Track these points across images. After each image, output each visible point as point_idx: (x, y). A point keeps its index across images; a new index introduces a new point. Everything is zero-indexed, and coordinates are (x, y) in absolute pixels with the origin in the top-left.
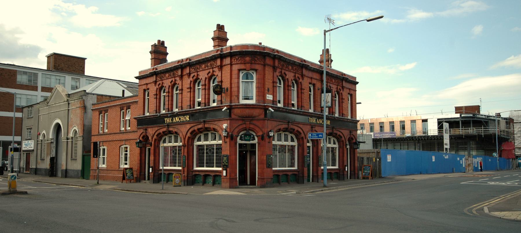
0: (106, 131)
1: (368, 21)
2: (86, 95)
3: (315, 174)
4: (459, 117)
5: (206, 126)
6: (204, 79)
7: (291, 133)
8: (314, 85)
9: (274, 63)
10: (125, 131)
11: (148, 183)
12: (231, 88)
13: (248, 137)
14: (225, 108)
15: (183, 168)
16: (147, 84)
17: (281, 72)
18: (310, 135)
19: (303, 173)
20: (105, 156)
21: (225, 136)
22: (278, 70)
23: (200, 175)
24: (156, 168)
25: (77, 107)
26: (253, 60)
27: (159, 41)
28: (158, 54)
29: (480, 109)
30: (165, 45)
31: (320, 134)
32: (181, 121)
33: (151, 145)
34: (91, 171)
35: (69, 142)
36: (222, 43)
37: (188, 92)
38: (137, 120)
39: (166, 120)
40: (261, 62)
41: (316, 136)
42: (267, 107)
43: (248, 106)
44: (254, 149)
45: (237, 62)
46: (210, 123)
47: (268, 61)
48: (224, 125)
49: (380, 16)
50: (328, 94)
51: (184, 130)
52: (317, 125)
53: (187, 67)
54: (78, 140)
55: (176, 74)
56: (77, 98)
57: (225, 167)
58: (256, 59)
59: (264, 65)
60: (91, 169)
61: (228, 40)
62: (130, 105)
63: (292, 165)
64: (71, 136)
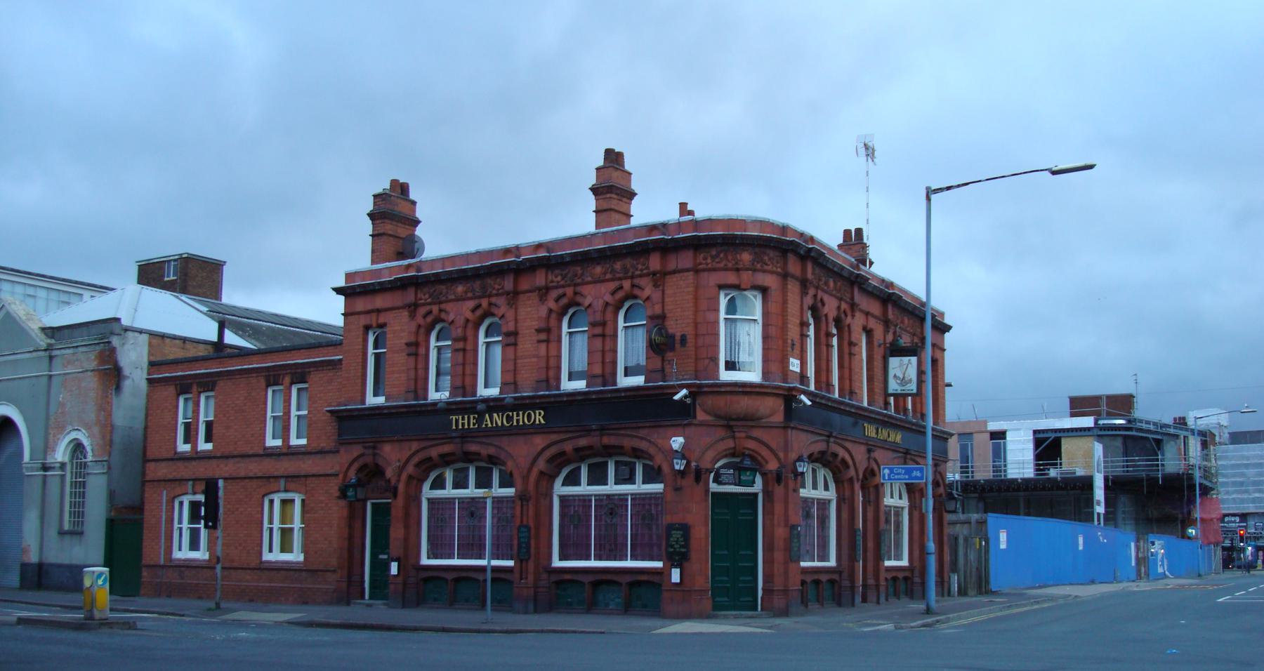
0: (204, 446)
1: (1054, 173)
2: (120, 335)
3: (871, 581)
4: (1093, 426)
5: (606, 440)
6: (461, 321)
7: (825, 465)
8: (869, 332)
9: (804, 270)
10: (285, 451)
11: (382, 607)
12: (697, 336)
13: (749, 476)
14: (684, 392)
15: (521, 561)
16: (379, 311)
17: (815, 296)
18: (887, 471)
19: (852, 577)
20: (297, 524)
21: (679, 471)
22: (812, 292)
23: (581, 582)
24: (408, 559)
25: (87, 371)
26: (758, 262)
27: (394, 183)
28: (395, 223)
29: (1135, 404)
30: (412, 197)
31: (917, 469)
32: (515, 424)
33: (395, 496)
34: (144, 569)
35: (49, 480)
36: (620, 202)
37: (539, 341)
38: (337, 417)
39: (457, 421)
40: (777, 268)
41: (905, 474)
42: (794, 393)
43: (748, 390)
44: (1089, 508)
45: (714, 263)
46: (622, 432)
47: (794, 266)
48: (673, 439)
49: (1089, 162)
50: (909, 360)
51: (521, 452)
52: (879, 445)
53: (538, 272)
54: (88, 474)
55: (494, 289)
56: (89, 340)
57: (678, 558)
58: (766, 258)
59: (785, 276)
60: (144, 562)
61: (636, 194)
62: (307, 370)
63: (824, 557)
64: (60, 459)
